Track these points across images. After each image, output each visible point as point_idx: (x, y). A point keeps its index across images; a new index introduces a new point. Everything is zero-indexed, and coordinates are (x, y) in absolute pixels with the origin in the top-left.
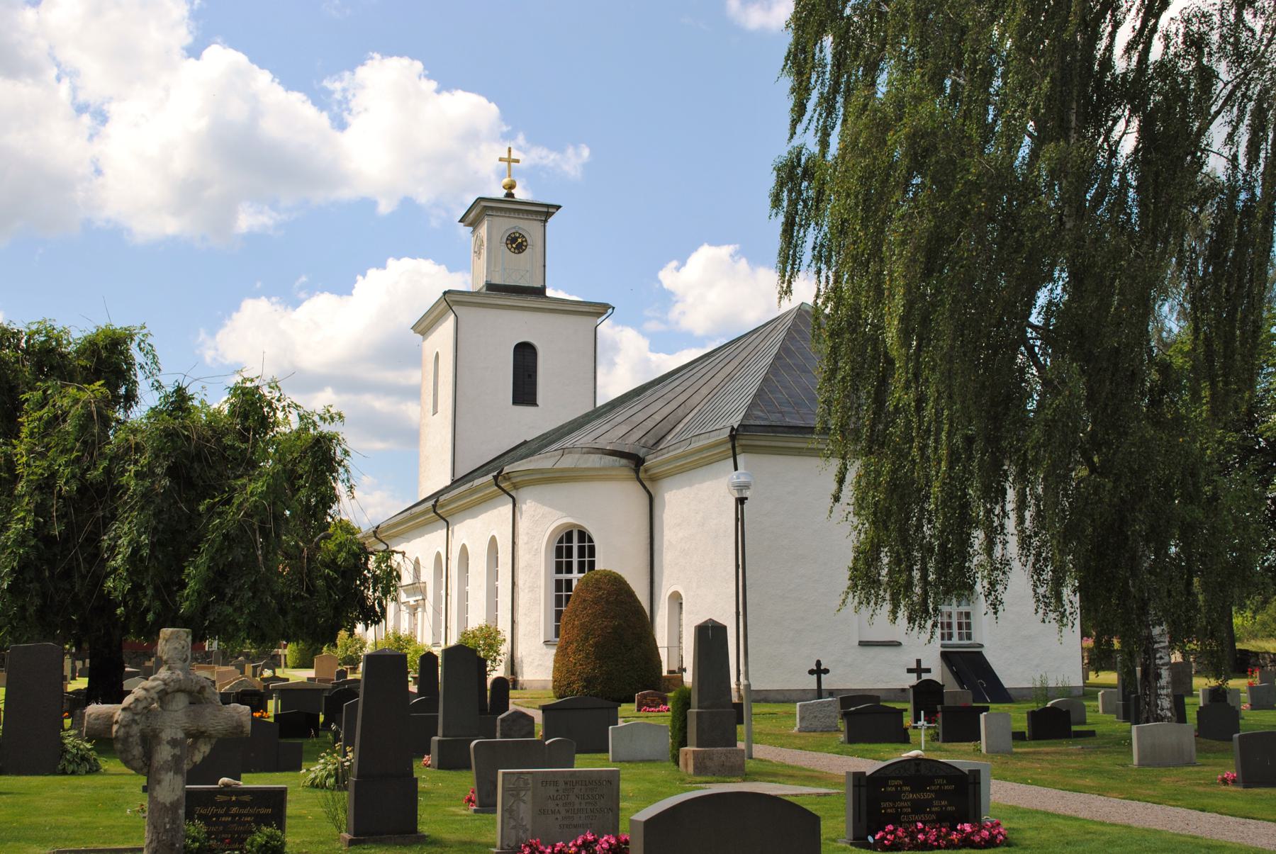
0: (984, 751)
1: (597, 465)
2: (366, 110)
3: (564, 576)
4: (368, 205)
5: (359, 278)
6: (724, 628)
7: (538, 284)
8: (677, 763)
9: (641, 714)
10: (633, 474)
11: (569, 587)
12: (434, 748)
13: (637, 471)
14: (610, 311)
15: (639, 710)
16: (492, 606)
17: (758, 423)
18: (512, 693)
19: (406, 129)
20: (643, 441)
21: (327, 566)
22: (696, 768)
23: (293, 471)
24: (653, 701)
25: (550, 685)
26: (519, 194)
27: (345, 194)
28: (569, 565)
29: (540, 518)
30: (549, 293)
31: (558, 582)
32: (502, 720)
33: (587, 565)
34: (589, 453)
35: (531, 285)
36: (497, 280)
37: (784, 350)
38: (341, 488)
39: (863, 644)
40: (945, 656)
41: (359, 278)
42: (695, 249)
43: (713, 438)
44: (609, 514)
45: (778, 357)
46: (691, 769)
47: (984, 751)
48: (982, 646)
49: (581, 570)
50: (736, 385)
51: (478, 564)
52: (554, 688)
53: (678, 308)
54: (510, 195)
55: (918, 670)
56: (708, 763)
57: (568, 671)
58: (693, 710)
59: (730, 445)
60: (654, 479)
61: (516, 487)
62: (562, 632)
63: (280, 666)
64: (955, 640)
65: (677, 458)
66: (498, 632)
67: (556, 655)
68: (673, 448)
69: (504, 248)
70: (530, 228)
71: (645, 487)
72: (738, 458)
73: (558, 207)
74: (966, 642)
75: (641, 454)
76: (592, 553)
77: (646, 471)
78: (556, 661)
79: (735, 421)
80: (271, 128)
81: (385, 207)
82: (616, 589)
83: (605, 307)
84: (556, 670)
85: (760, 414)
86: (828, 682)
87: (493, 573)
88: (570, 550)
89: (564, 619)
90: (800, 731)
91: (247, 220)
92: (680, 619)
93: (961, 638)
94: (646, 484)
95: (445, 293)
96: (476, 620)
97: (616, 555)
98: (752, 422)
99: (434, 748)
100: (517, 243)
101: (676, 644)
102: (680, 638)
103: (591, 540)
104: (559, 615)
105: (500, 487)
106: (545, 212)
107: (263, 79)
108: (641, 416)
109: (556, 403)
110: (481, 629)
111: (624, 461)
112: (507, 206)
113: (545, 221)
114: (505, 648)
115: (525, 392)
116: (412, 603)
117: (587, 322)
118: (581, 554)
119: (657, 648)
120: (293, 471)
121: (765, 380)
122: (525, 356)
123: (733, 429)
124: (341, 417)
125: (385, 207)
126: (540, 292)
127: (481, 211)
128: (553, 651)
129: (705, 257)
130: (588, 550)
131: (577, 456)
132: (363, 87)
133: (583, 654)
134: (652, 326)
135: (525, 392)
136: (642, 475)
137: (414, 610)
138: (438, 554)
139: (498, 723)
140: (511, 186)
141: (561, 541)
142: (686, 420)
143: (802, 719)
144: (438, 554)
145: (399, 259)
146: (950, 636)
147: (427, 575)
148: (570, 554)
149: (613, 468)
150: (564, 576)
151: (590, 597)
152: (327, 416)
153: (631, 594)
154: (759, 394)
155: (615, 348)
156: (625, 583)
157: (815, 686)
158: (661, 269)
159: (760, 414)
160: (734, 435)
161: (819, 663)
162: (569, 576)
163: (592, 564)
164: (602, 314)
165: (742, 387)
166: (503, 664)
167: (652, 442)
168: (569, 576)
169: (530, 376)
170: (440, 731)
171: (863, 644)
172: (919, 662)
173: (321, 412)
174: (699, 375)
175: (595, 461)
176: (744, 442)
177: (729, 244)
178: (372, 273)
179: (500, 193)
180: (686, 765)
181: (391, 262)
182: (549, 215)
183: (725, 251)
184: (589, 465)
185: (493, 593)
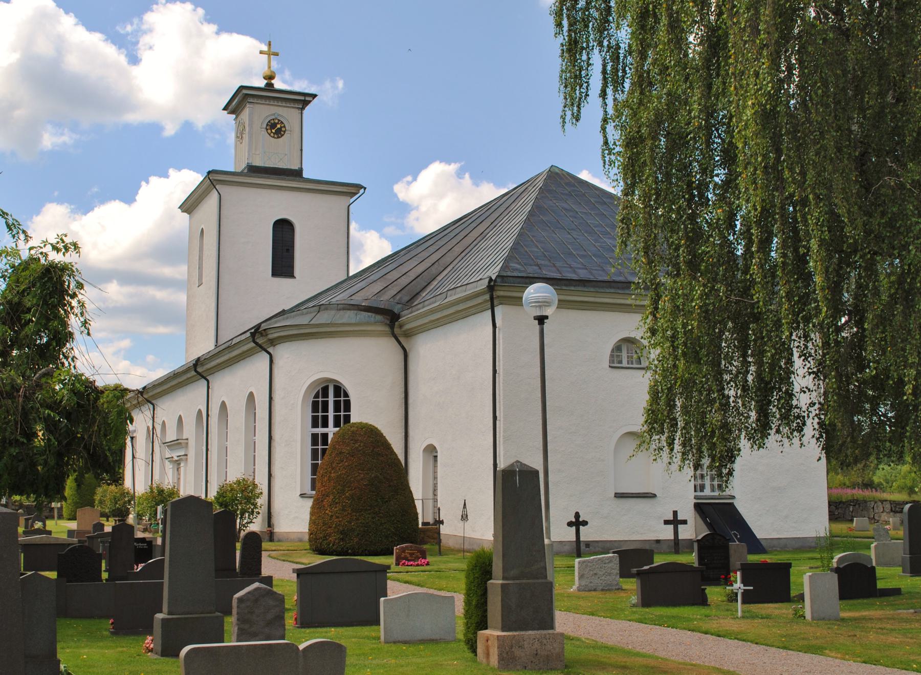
0: (808, 616)
1: (353, 321)
2: (151, 48)
3: (320, 430)
4: (155, 128)
5: (143, 183)
6: (537, 472)
7: (296, 168)
8: (474, 650)
9: (400, 568)
10: (387, 329)
11: (325, 442)
12: (157, 628)
13: (392, 327)
14: (362, 191)
15: (398, 564)
16: (252, 460)
17: (515, 274)
18: (265, 545)
19: (185, 66)
20: (398, 297)
21: (50, 407)
22: (501, 659)
23: (19, 303)
24: (411, 554)
25: (307, 537)
26: (278, 84)
27: (132, 118)
28: (325, 419)
29: (300, 368)
30: (305, 175)
31: (314, 437)
32: (240, 600)
33: (343, 420)
34: (344, 309)
35: (289, 167)
36: (258, 162)
37: (537, 209)
38: (74, 323)
39: (619, 496)
40: (699, 507)
41: (143, 183)
42: (426, 166)
43: (470, 290)
44: (361, 367)
45: (531, 214)
46: (494, 660)
47: (808, 616)
48: (733, 497)
49: (337, 424)
50: (490, 242)
51: (237, 417)
52: (310, 540)
53: (414, 214)
54: (270, 86)
55: (675, 522)
56: (517, 652)
57: (324, 524)
58: (496, 582)
59: (487, 297)
60: (409, 334)
61: (273, 342)
62: (318, 485)
63: (52, 517)
64: (707, 492)
65: (432, 311)
66: (255, 486)
67: (313, 508)
68: (428, 303)
69: (264, 132)
70: (287, 114)
71: (400, 343)
72: (496, 309)
73: (314, 96)
74: (716, 493)
75: (393, 307)
76: (348, 405)
77: (401, 327)
78: (312, 514)
79: (493, 272)
80: (73, 63)
81: (170, 130)
82: (372, 438)
83: (359, 187)
84: (312, 522)
85: (519, 267)
86: (586, 534)
87: (252, 430)
88: (325, 404)
89: (320, 471)
90: (579, 590)
91: (48, 140)
92: (435, 472)
93: (713, 490)
94: (401, 339)
95: (209, 173)
96: (235, 474)
97: (370, 408)
98: (509, 274)
99: (157, 628)
100: (276, 129)
101: (431, 496)
102: (435, 490)
103: (346, 395)
104: (315, 468)
105: (256, 343)
106: (303, 100)
107: (68, 23)
108: (395, 275)
109: (312, 275)
110: (238, 482)
111: (379, 317)
112: (268, 93)
113: (303, 109)
114: (262, 501)
115: (283, 265)
116: (176, 458)
117: (343, 201)
118: (337, 408)
119: (413, 500)
120: (19, 303)
121: (520, 234)
122: (283, 231)
123: (491, 280)
124: (75, 246)
125: (170, 130)
126: (297, 174)
127: (241, 100)
128: (309, 503)
129: (435, 171)
130: (344, 404)
131: (333, 312)
132: (151, 31)
133: (339, 507)
134: (389, 230)
135: (283, 265)
136: (396, 330)
137: (177, 463)
138: (200, 412)
139: (235, 603)
140: (270, 77)
141: (317, 396)
142: (439, 278)
143: (581, 577)
144: (200, 412)
145: (180, 170)
146: (702, 488)
147: (190, 431)
148: (325, 409)
149: (368, 324)
150: (320, 430)
151: (346, 449)
152: (61, 246)
153: (387, 446)
154: (515, 248)
155: (361, 246)
156: (381, 435)
157: (573, 538)
158: (397, 183)
159: (519, 267)
160: (492, 286)
161: (577, 515)
162: (324, 430)
163: (347, 418)
164: (355, 194)
165: (496, 243)
166: (260, 517)
167: (407, 298)
168: (324, 430)
169: (288, 250)
170: (165, 607)
171: (619, 496)
172: (675, 513)
173: (54, 241)
174: (452, 234)
175: (350, 316)
176: (501, 293)
177: (455, 162)
178: (154, 180)
179: (262, 83)
180: (488, 655)
181: (171, 172)
182: (306, 103)
183: (453, 167)
184: (344, 321)
185: (251, 447)
